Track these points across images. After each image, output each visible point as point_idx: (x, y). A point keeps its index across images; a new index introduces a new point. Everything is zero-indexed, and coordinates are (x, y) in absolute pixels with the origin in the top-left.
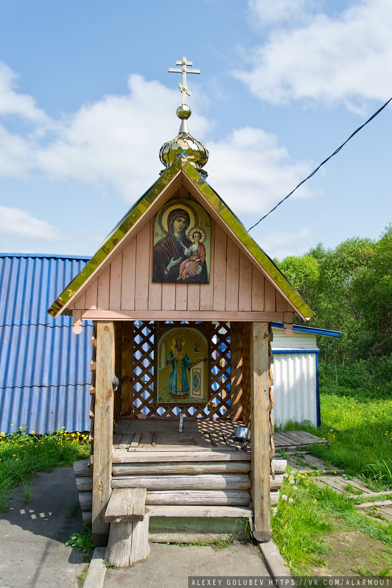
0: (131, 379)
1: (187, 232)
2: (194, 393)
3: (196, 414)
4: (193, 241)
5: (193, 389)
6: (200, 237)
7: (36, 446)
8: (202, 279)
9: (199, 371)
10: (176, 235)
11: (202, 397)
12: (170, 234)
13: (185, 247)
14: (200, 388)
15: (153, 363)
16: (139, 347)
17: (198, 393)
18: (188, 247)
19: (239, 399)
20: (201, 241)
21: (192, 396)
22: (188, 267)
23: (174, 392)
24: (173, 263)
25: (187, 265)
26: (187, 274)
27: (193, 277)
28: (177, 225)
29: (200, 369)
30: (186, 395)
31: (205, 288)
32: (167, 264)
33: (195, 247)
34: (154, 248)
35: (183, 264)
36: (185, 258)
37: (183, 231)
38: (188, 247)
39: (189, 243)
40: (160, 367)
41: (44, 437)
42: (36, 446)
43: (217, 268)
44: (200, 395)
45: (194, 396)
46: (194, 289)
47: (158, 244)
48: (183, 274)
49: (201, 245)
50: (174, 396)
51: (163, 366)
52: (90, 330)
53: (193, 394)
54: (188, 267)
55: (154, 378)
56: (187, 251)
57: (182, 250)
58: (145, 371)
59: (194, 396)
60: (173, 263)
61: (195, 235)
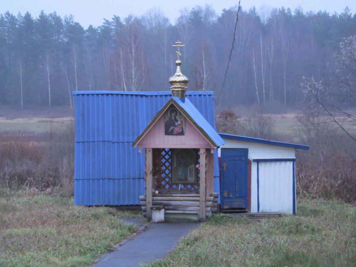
0: (161, 172)
1: (176, 117)
2: (190, 178)
3: (191, 188)
4: (178, 120)
5: (190, 177)
6: (181, 119)
7: (156, 184)
8: (182, 133)
9: (192, 168)
10: (173, 118)
11: (193, 180)
12: (171, 118)
13: (269, 115)
14: (193, 176)
15: (171, 164)
16: (164, 157)
17: (192, 178)
18: (177, 122)
19: (192, 194)
20: (181, 120)
21: (189, 179)
22: (177, 130)
23: (180, 178)
24: (172, 128)
25: (177, 129)
26: (177, 132)
27: (179, 133)
28: (173, 115)
29: (193, 167)
30: (186, 179)
31: (183, 137)
32: (170, 128)
33: (179, 122)
34: (165, 123)
35: (175, 128)
36: (176, 126)
37: (175, 118)
38: (177, 122)
39: (177, 121)
40: (174, 166)
41: (70, 217)
42: (156, 184)
43: (187, 131)
44: (193, 179)
45: (190, 180)
46: (179, 137)
47: (167, 121)
48: (175, 132)
49: (182, 122)
50: (180, 180)
51: (175, 166)
52: (144, 151)
53: (189, 179)
54: (177, 130)
55: (171, 172)
56: (176, 124)
57: (175, 123)
58: (167, 168)
59: (190, 180)
60: (172, 128)
61: (180, 118)
